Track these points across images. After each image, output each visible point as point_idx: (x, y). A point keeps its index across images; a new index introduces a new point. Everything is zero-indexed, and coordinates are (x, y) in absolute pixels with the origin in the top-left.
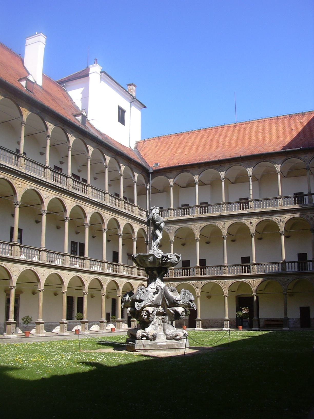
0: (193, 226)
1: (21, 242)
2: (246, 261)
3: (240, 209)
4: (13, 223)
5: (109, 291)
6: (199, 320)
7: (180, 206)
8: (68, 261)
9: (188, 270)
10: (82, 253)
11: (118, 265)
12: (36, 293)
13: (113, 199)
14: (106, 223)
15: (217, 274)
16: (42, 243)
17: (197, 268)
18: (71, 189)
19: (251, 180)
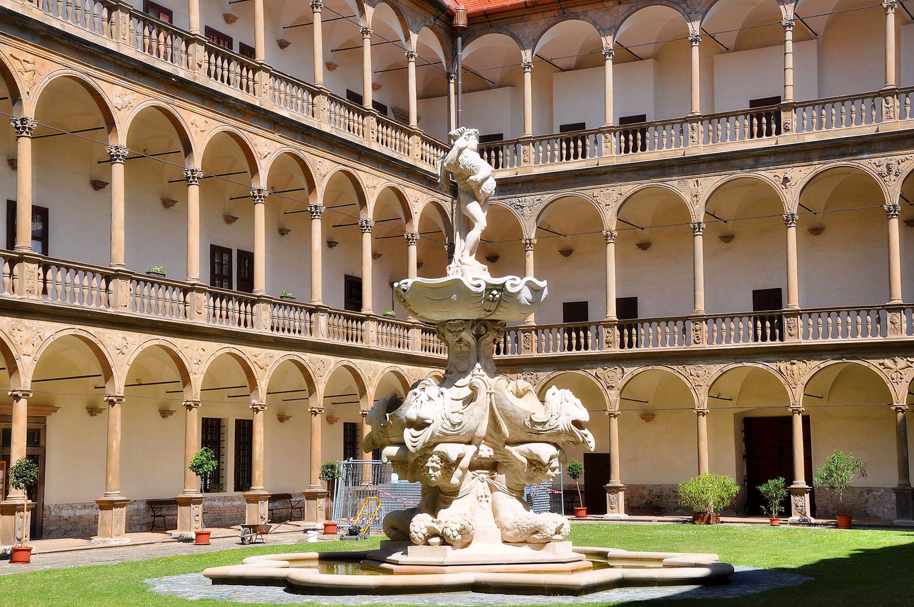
0: (596, 192)
1: (45, 251)
2: (768, 302)
3: (752, 136)
4: (15, 185)
5: (334, 400)
6: (616, 489)
7: (557, 131)
8: (201, 310)
9: (582, 334)
10: (247, 283)
11: (362, 320)
12: (100, 411)
13: (343, 112)
14: (321, 187)
15: (672, 344)
16: (114, 251)
17: (609, 325)
18: (202, 79)
19: (789, 35)
